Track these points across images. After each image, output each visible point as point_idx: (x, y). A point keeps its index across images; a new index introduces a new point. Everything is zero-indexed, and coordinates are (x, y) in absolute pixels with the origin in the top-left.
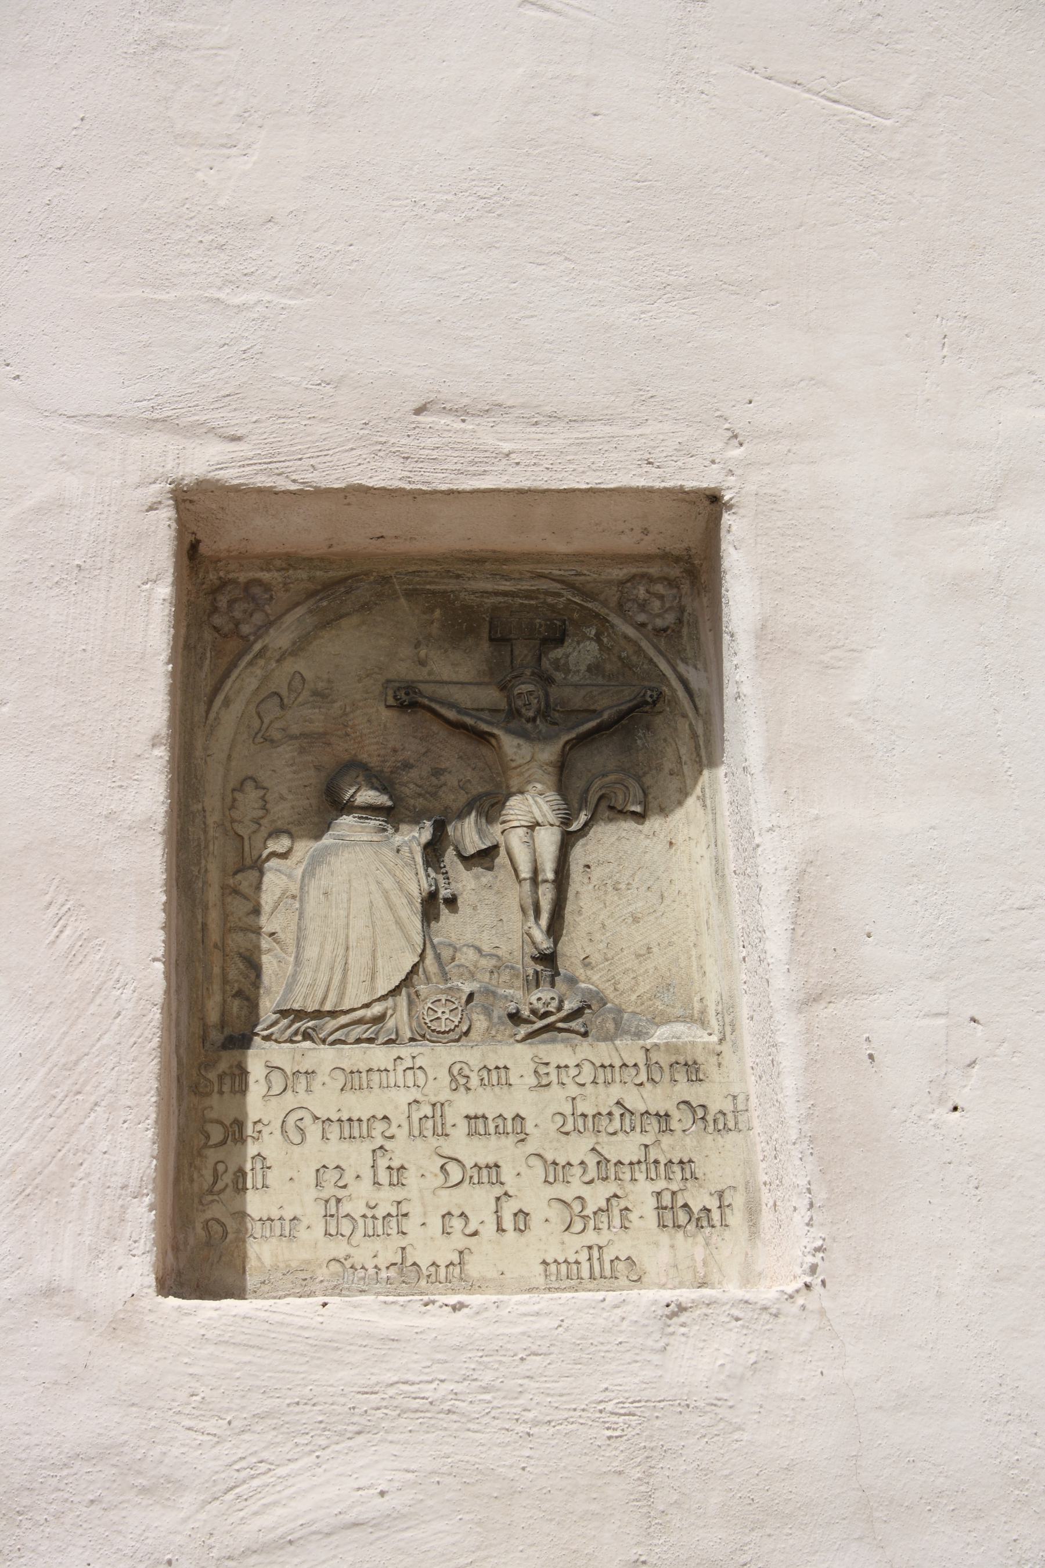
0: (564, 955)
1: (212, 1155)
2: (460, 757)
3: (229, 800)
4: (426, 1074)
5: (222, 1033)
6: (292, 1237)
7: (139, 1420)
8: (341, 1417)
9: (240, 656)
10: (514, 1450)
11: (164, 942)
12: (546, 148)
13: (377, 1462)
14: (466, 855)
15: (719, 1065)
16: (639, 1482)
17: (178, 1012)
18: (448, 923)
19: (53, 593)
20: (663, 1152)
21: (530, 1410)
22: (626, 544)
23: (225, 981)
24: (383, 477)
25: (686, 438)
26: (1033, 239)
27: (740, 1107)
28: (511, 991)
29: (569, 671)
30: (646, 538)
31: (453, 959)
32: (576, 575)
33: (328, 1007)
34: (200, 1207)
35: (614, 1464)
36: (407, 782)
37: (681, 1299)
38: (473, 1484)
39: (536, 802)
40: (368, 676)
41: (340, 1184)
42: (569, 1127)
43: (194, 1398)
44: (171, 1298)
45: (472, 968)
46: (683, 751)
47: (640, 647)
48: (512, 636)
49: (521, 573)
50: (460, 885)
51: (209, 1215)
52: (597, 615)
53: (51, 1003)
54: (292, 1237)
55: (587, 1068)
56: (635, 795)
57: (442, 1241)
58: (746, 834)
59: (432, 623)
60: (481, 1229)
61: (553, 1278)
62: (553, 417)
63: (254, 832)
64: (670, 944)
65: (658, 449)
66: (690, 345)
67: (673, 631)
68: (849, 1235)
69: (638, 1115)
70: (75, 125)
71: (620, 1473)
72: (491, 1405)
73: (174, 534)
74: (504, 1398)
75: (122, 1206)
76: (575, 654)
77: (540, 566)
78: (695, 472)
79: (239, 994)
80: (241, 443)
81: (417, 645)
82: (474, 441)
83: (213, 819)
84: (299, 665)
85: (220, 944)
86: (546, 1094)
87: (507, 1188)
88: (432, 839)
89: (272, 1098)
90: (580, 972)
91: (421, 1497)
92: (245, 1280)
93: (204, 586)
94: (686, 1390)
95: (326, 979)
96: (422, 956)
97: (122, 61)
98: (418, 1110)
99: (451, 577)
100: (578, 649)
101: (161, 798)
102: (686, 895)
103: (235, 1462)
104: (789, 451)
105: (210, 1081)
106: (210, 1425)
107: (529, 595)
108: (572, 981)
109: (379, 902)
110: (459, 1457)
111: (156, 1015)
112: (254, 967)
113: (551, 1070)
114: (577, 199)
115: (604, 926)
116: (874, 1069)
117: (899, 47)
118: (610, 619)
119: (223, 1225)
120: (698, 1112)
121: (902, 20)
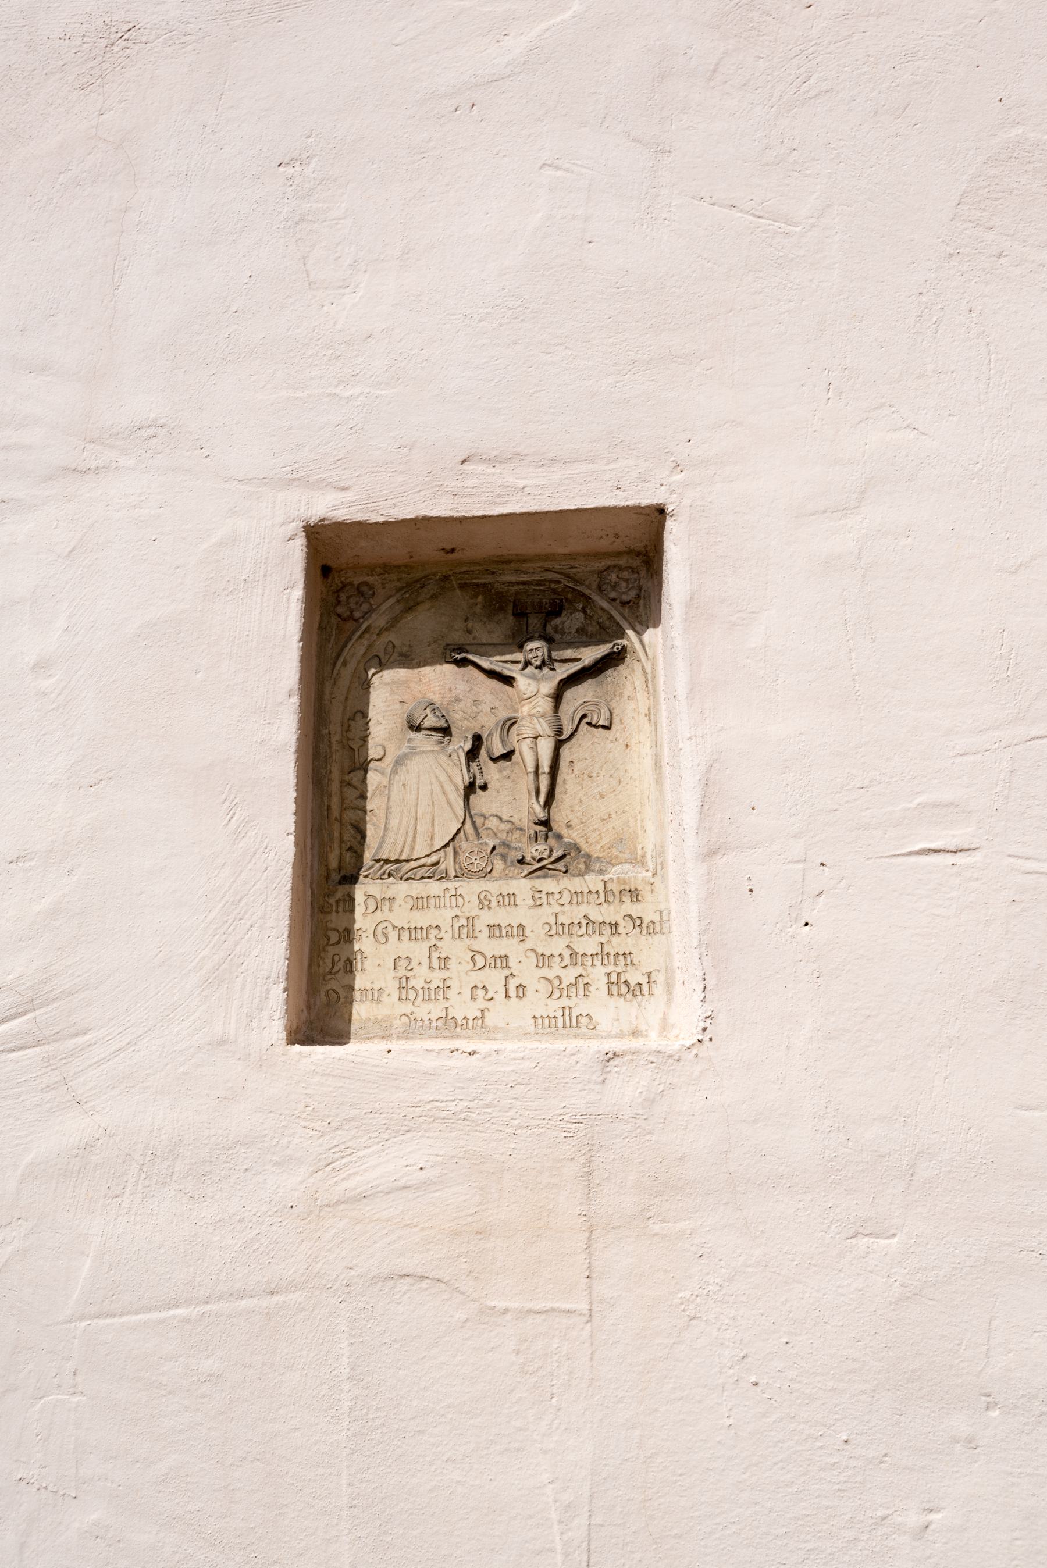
0: (554, 821)
1: (331, 950)
2: (492, 693)
3: (346, 726)
4: (463, 899)
5: (339, 874)
6: (378, 1001)
7: (275, 1121)
8: (397, 1121)
9: (353, 633)
10: (505, 1144)
11: (295, 822)
12: (555, 269)
13: (419, 1149)
14: (493, 757)
15: (652, 891)
16: (584, 1166)
17: (312, 861)
18: (478, 799)
19: (229, 598)
20: (613, 947)
21: (515, 1119)
22: (604, 545)
23: (342, 841)
24: (439, 509)
25: (644, 470)
26: (899, 307)
27: (665, 918)
28: (520, 845)
29: (565, 633)
30: (617, 540)
31: (484, 824)
32: (570, 568)
33: (403, 857)
34: (324, 982)
35: (568, 1154)
36: (458, 711)
37: (616, 1050)
38: (478, 1165)
39: (539, 721)
40: (434, 642)
41: (409, 968)
42: (553, 932)
43: (308, 1108)
44: (297, 1046)
45: (495, 830)
46: (637, 683)
47: (611, 615)
48: (528, 611)
49: (534, 569)
50: (489, 777)
51: (329, 987)
52: (584, 595)
53: (225, 863)
54: (378, 1001)
55: (566, 894)
56: (605, 714)
57: (470, 1003)
58: (675, 740)
59: (476, 604)
60: (495, 996)
61: (540, 1027)
62: (554, 460)
63: (361, 746)
64: (624, 812)
65: (625, 478)
66: (649, 403)
67: (634, 603)
68: (729, 1008)
69: (598, 924)
70: (246, 281)
71: (572, 1159)
72: (491, 1116)
73: (305, 555)
74: (500, 1111)
75: (267, 989)
76: (569, 621)
77: (546, 563)
78: (649, 493)
79: (350, 849)
80: (348, 492)
81: (466, 620)
82: (501, 480)
83: (335, 739)
84: (391, 636)
85: (339, 819)
86: (540, 910)
87: (512, 970)
88: (472, 748)
89: (368, 915)
90: (564, 832)
91: (446, 1172)
92: (350, 1027)
93: (332, 588)
94: (616, 1108)
95: (403, 839)
96: (463, 823)
97: (275, 235)
98: (458, 921)
99: (489, 574)
100: (570, 618)
101: (294, 730)
102: (635, 780)
103: (332, 1148)
104: (715, 474)
105: (331, 904)
106: (317, 1125)
107: (539, 583)
108: (559, 837)
109: (437, 789)
110: (470, 1148)
111: (289, 870)
112: (361, 833)
113: (543, 895)
114: (576, 304)
115: (581, 801)
116: (752, 899)
117: (808, 172)
118: (591, 597)
119: (337, 993)
120: (637, 922)
121: (811, 152)
